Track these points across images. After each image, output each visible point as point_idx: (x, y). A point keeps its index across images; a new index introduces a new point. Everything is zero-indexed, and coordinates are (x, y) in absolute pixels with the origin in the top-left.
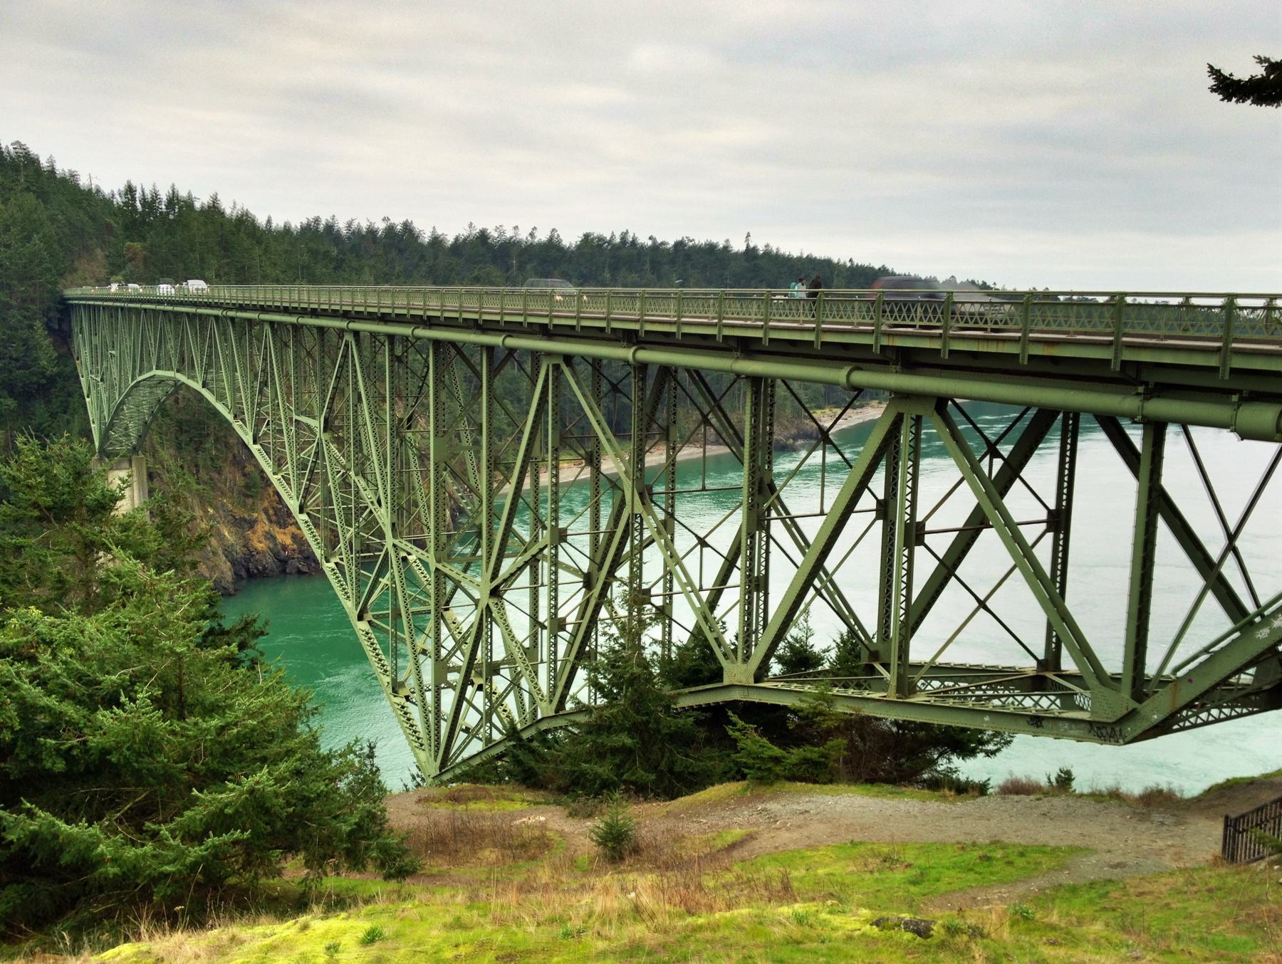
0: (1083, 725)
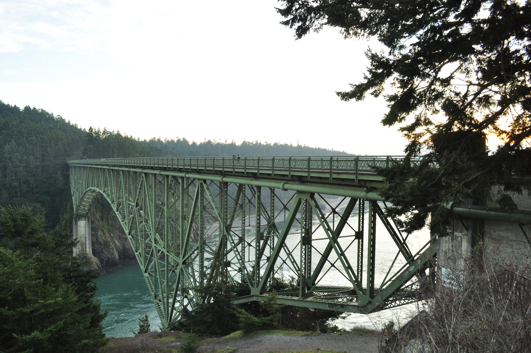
0: (356, 307)
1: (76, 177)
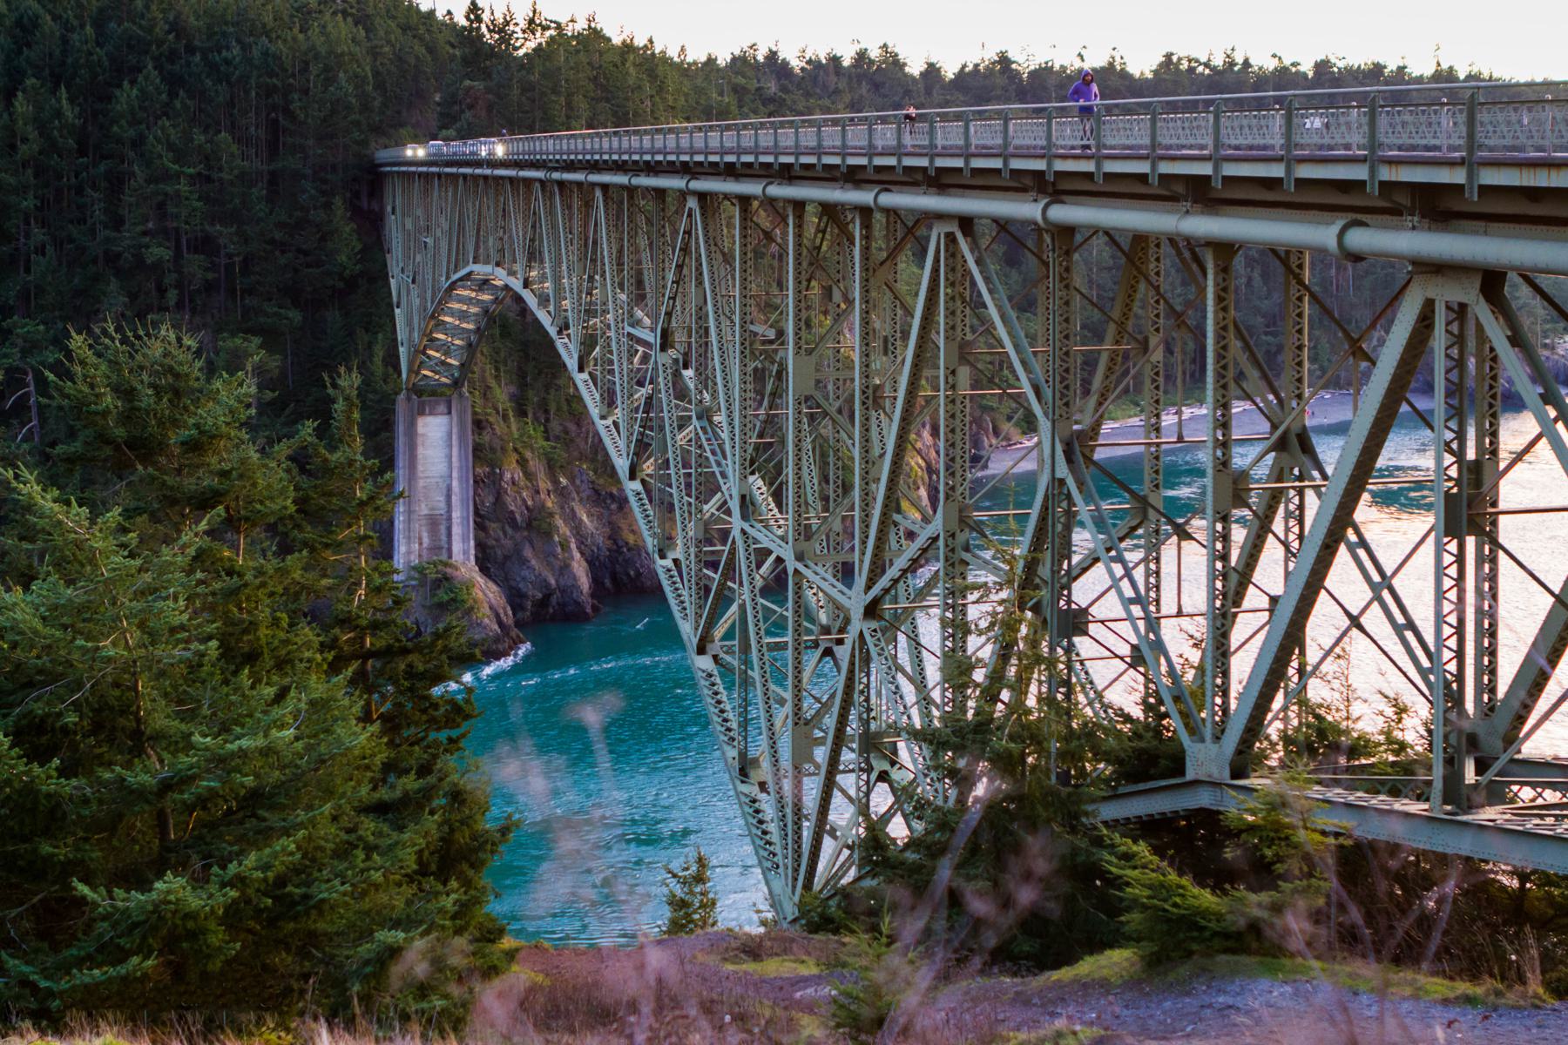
1: (409, 225)
